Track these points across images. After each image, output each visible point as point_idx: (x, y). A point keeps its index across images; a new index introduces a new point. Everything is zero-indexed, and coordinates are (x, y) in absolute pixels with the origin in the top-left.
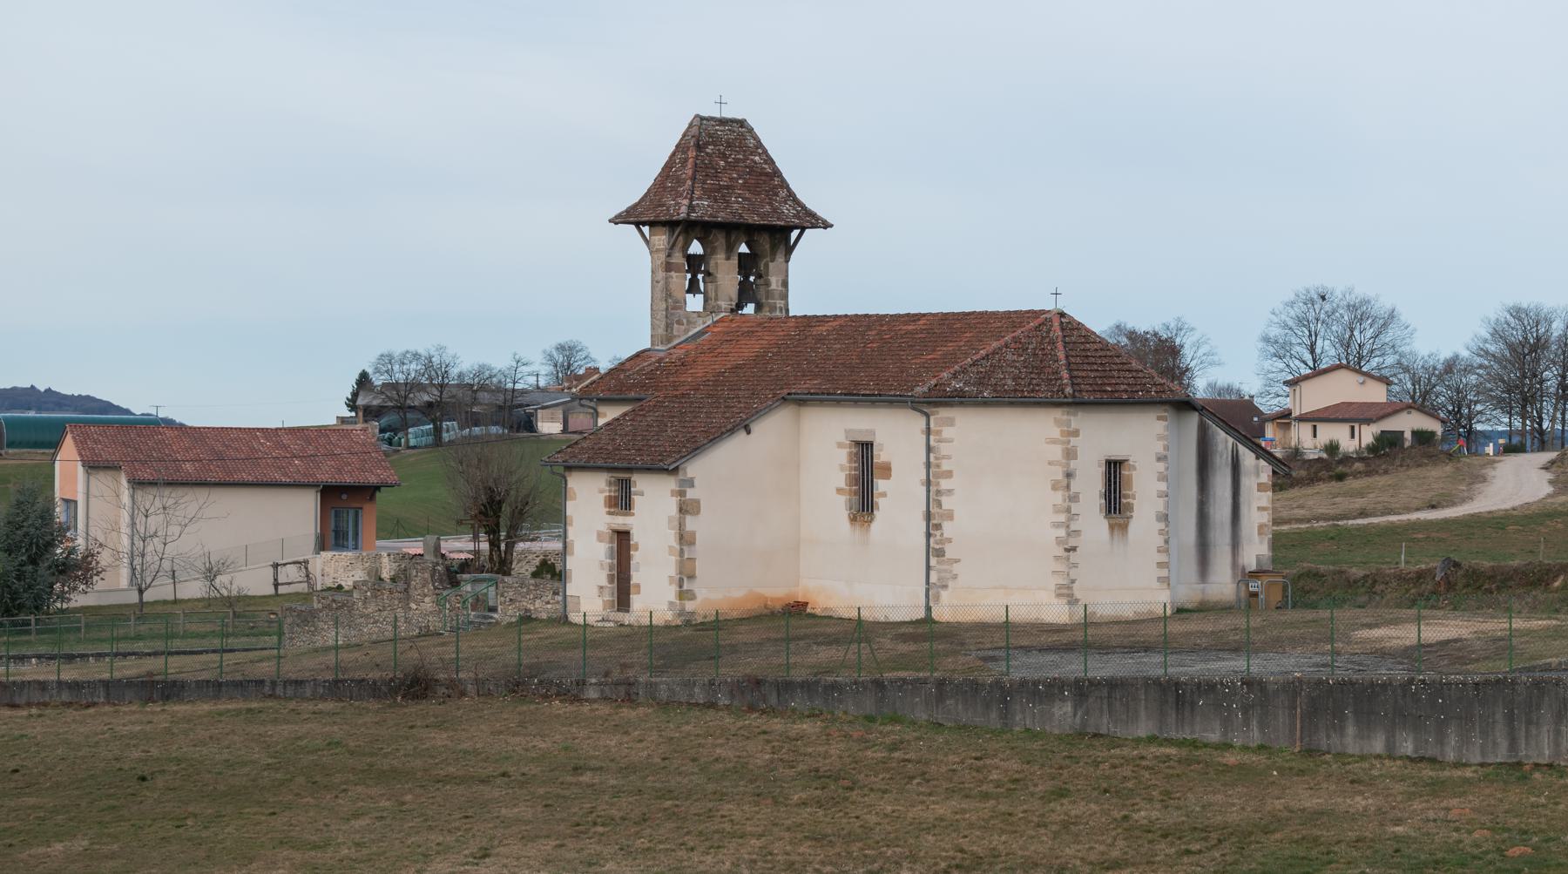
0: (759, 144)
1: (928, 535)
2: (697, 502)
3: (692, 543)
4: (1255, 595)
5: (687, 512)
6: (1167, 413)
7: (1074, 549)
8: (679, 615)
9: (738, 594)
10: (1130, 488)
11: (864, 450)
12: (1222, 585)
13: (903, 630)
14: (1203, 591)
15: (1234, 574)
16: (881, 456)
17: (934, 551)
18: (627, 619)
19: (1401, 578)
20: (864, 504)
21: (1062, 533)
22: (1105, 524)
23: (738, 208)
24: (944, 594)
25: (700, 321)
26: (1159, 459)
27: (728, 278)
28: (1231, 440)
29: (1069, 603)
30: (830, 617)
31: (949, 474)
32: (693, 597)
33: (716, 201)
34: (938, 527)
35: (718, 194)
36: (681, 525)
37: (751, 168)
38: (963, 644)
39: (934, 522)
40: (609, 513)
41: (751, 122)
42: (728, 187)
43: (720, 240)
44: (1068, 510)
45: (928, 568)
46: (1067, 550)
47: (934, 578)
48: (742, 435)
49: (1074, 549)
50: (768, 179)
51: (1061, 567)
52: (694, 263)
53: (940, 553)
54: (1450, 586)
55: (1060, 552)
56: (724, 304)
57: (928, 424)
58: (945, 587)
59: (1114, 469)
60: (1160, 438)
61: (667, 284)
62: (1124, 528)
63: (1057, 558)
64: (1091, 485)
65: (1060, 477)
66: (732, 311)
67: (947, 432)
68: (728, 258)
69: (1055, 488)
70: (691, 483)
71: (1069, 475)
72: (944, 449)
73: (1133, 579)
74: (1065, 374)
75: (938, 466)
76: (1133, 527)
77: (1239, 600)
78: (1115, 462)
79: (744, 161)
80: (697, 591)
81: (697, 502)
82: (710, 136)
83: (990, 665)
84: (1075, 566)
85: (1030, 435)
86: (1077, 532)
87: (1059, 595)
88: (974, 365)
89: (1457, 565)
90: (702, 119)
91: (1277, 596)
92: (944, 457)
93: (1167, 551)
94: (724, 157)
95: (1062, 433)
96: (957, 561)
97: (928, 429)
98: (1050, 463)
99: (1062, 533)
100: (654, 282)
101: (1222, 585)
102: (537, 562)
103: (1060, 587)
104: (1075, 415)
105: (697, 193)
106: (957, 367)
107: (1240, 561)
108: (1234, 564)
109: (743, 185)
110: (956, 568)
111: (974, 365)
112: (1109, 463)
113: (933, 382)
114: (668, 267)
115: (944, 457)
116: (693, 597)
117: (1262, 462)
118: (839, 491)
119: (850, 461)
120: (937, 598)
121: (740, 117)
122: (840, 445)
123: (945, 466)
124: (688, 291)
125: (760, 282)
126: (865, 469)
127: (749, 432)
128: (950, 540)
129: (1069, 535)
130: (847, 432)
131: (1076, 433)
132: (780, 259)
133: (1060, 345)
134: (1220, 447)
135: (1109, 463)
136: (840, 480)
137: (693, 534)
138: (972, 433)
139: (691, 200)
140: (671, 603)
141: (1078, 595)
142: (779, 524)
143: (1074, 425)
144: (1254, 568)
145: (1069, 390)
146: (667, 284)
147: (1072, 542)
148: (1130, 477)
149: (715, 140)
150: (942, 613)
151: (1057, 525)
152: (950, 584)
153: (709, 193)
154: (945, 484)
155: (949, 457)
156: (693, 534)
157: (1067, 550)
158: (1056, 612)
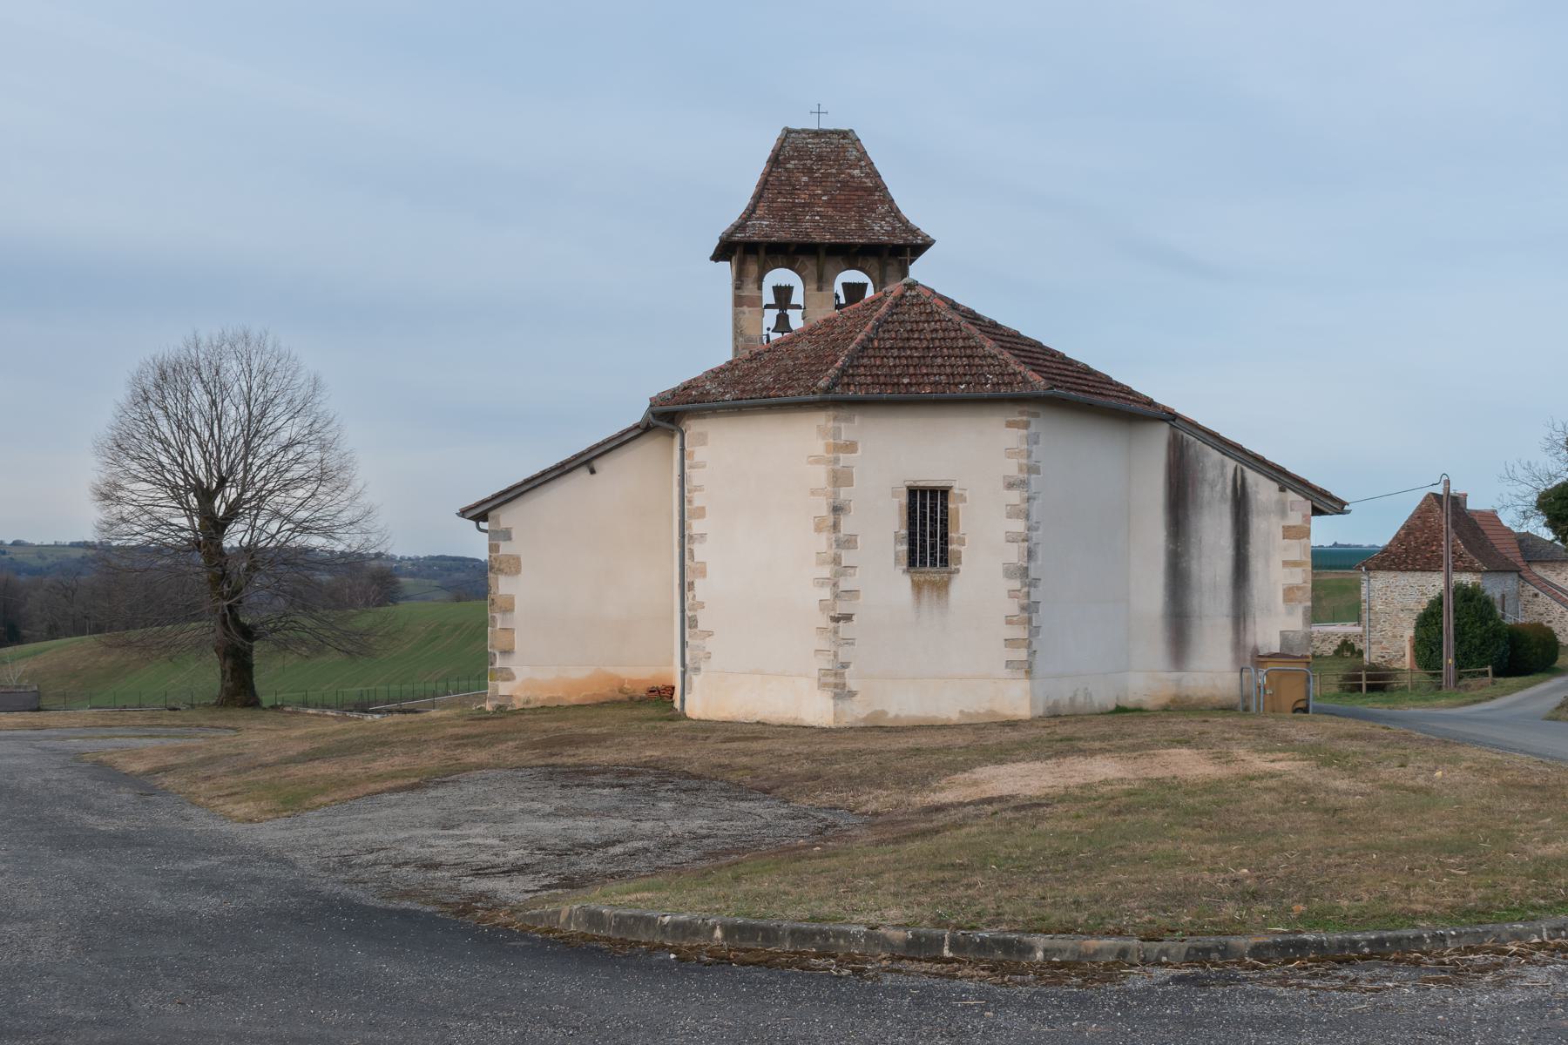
2: (517, 559)
6: (1014, 414)
7: (848, 618)
14: (1178, 682)
21: (826, 593)
22: (906, 581)
28: (1231, 464)
29: (836, 696)
33: (782, 219)
37: (845, 184)
42: (804, 205)
44: (836, 560)
46: (836, 620)
48: (583, 473)
49: (848, 618)
53: (694, 623)
55: (824, 621)
60: (1010, 453)
62: (942, 587)
64: (882, 526)
65: (824, 511)
69: (818, 529)
70: (507, 535)
71: (837, 509)
73: (950, 664)
78: (923, 491)
79: (835, 175)
80: (514, 669)
82: (796, 149)
84: (849, 642)
86: (853, 593)
94: (809, 171)
95: (828, 448)
96: (710, 634)
102: (1339, 642)
104: (849, 420)
107: (1250, 640)
108: (1238, 644)
109: (828, 202)
110: (710, 645)
117: (1291, 496)
121: (845, 128)
123: (697, 503)
126: (928, 526)
127: (593, 472)
129: (836, 596)
131: (850, 447)
134: (1211, 474)
135: (912, 492)
141: (852, 684)
144: (1276, 650)
147: (842, 608)
149: (801, 153)
151: (820, 582)
157: (836, 620)
158: (817, 710)
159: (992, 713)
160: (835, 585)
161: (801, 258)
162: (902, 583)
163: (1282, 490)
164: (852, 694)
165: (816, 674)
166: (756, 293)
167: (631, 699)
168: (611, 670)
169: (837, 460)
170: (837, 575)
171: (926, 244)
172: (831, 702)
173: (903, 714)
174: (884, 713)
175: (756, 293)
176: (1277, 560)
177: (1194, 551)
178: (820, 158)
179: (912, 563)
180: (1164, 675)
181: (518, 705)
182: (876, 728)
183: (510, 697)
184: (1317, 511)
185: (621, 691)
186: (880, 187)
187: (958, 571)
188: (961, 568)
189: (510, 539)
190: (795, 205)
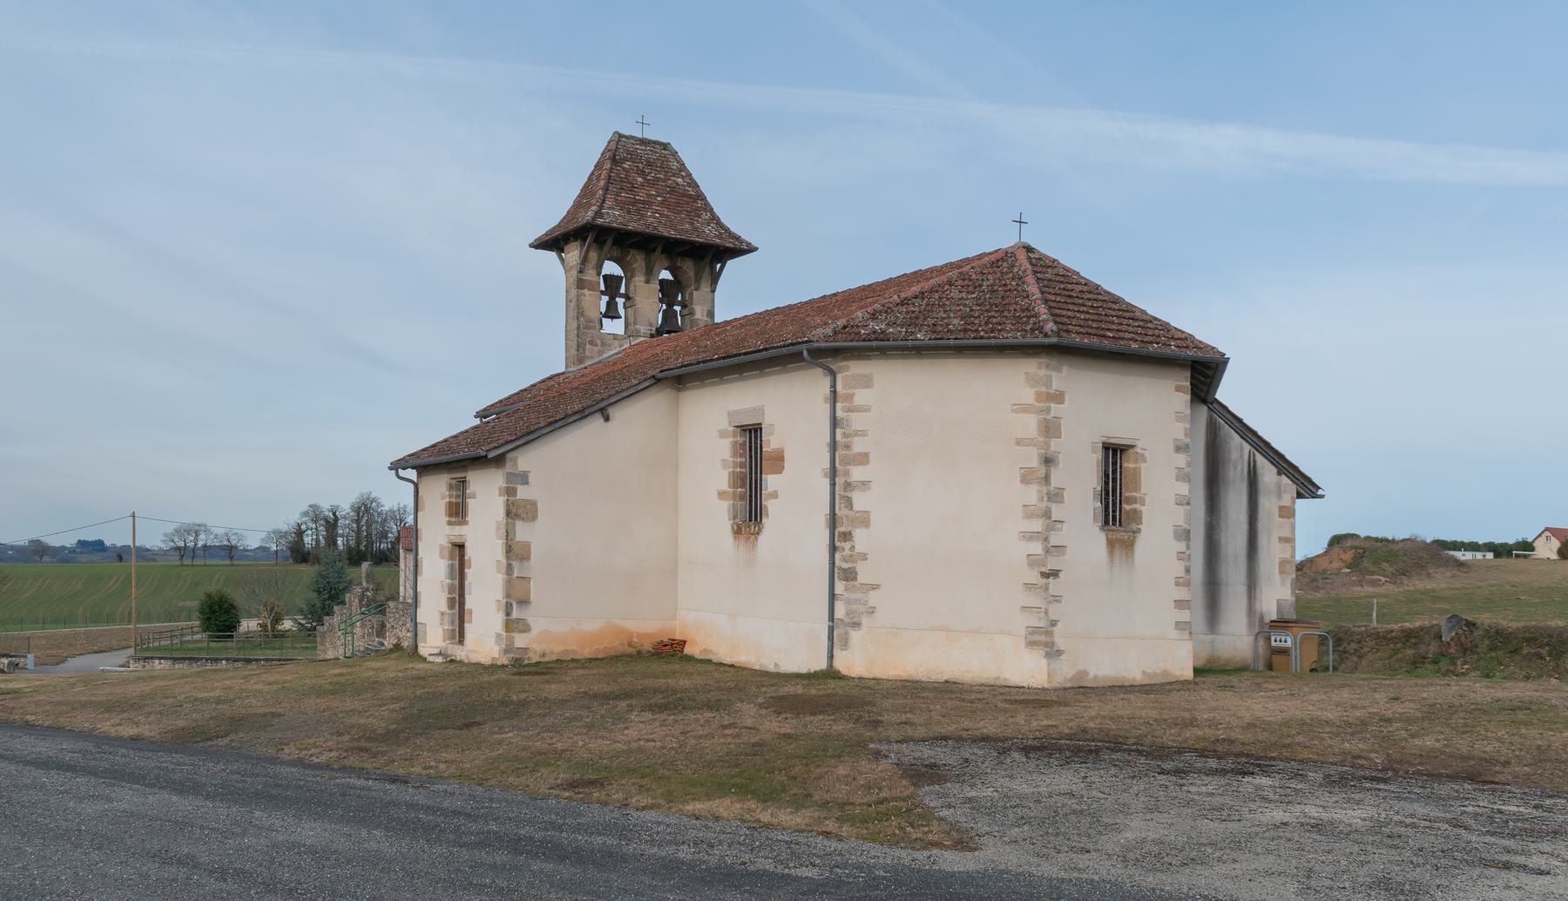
0: (682, 167)
1: (833, 549)
2: (534, 504)
3: (525, 557)
4: (1284, 652)
5: (517, 516)
7: (1054, 574)
8: (506, 651)
9: (592, 626)
10: (1137, 488)
11: (752, 433)
12: (1236, 639)
13: (789, 689)
14: (1212, 643)
15: (1251, 624)
16: (771, 442)
17: (840, 572)
18: (460, 653)
19: (1382, 638)
20: (750, 511)
21: (1037, 548)
22: (1101, 538)
23: (654, 221)
24: (855, 635)
25: (616, 343)
26: (1178, 449)
27: (651, 309)
28: (1247, 447)
29: (1048, 655)
30: (709, 661)
31: (863, 459)
32: (524, 627)
33: (629, 212)
34: (847, 536)
35: (629, 206)
36: (509, 535)
38: (876, 724)
39: (840, 529)
40: (450, 523)
41: (676, 146)
42: (644, 202)
43: (639, 261)
44: (1047, 514)
45: (832, 597)
46: (1045, 575)
47: (840, 611)
48: (597, 421)
49: (1054, 574)
50: (691, 199)
51: (1035, 600)
52: (612, 283)
53: (850, 575)
54: (1466, 650)
55: (1034, 577)
56: (643, 329)
57: (834, 385)
58: (857, 625)
59: (1114, 454)
61: (579, 303)
63: (1029, 586)
65: (1034, 462)
66: (652, 336)
67: (861, 397)
68: (647, 282)
69: (1025, 480)
70: (524, 478)
71: (1048, 461)
72: (857, 421)
74: (1042, 309)
75: (848, 447)
76: (1142, 546)
77: (1256, 658)
80: (530, 620)
81: (534, 504)
82: (628, 152)
83: (929, 796)
84: (1057, 599)
85: (998, 394)
87: (1031, 644)
88: (902, 303)
89: (1471, 625)
90: (621, 136)
91: (1312, 655)
92: (857, 433)
93: (1187, 584)
94: (642, 173)
95: (1038, 395)
96: (875, 587)
97: (834, 392)
98: (1019, 442)
99: (1037, 548)
100: (568, 301)
101: (1236, 639)
103: (1034, 630)
104: (1058, 370)
105: (608, 203)
106: (877, 306)
107: (1258, 606)
108: (1251, 610)
109: (662, 203)
110: (873, 598)
111: (902, 303)
112: (1107, 447)
113: (841, 323)
114: (581, 284)
115: (857, 433)
116: (524, 627)
117: (1285, 480)
118: (721, 495)
119: (734, 455)
120: (845, 644)
122: (723, 434)
123: (859, 446)
124: (606, 316)
125: (686, 311)
126: (753, 453)
127: (607, 419)
128: (864, 557)
129: (1047, 551)
130: (730, 414)
131: (1059, 398)
132: (705, 288)
133: (1030, 279)
134: (1234, 455)
135: (1107, 447)
136: (721, 479)
137: (527, 546)
138: (890, 393)
139: (601, 207)
140: (498, 635)
141: (1061, 643)
142: (685, 551)
143: (1056, 385)
144: (1274, 617)
145: (1050, 326)
146: (579, 303)
147: (1052, 564)
148: (1137, 472)
149: (633, 156)
150: (855, 662)
151: (1029, 537)
152: (865, 620)
153: (620, 204)
154: (857, 473)
155: (863, 433)
156: (527, 546)
157: (1045, 575)
158: (1027, 669)
159: (1165, 673)
160: (1046, 539)
161: (632, 252)
162: (1099, 539)
163: (1279, 474)
164: (1059, 653)
165: (1023, 633)
166: (594, 278)
167: (639, 652)
168: (620, 623)
169: (1048, 410)
170: (1049, 528)
171: (737, 249)
172: (1044, 662)
173: (1101, 674)
174: (1085, 673)
175: (594, 278)
176: (1275, 538)
177: (1223, 525)
178: (649, 164)
179: (1106, 522)
180: (1202, 637)
181: (535, 659)
182: (1081, 691)
183: (526, 650)
184: (1300, 496)
185: (630, 645)
186: (700, 196)
187: (1139, 531)
188: (1142, 527)
189: (526, 483)
190: (637, 201)
